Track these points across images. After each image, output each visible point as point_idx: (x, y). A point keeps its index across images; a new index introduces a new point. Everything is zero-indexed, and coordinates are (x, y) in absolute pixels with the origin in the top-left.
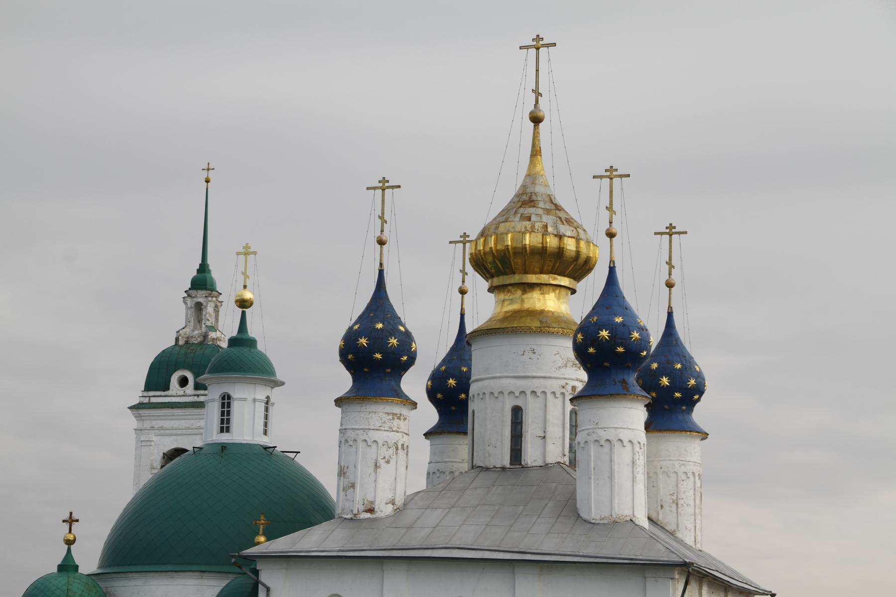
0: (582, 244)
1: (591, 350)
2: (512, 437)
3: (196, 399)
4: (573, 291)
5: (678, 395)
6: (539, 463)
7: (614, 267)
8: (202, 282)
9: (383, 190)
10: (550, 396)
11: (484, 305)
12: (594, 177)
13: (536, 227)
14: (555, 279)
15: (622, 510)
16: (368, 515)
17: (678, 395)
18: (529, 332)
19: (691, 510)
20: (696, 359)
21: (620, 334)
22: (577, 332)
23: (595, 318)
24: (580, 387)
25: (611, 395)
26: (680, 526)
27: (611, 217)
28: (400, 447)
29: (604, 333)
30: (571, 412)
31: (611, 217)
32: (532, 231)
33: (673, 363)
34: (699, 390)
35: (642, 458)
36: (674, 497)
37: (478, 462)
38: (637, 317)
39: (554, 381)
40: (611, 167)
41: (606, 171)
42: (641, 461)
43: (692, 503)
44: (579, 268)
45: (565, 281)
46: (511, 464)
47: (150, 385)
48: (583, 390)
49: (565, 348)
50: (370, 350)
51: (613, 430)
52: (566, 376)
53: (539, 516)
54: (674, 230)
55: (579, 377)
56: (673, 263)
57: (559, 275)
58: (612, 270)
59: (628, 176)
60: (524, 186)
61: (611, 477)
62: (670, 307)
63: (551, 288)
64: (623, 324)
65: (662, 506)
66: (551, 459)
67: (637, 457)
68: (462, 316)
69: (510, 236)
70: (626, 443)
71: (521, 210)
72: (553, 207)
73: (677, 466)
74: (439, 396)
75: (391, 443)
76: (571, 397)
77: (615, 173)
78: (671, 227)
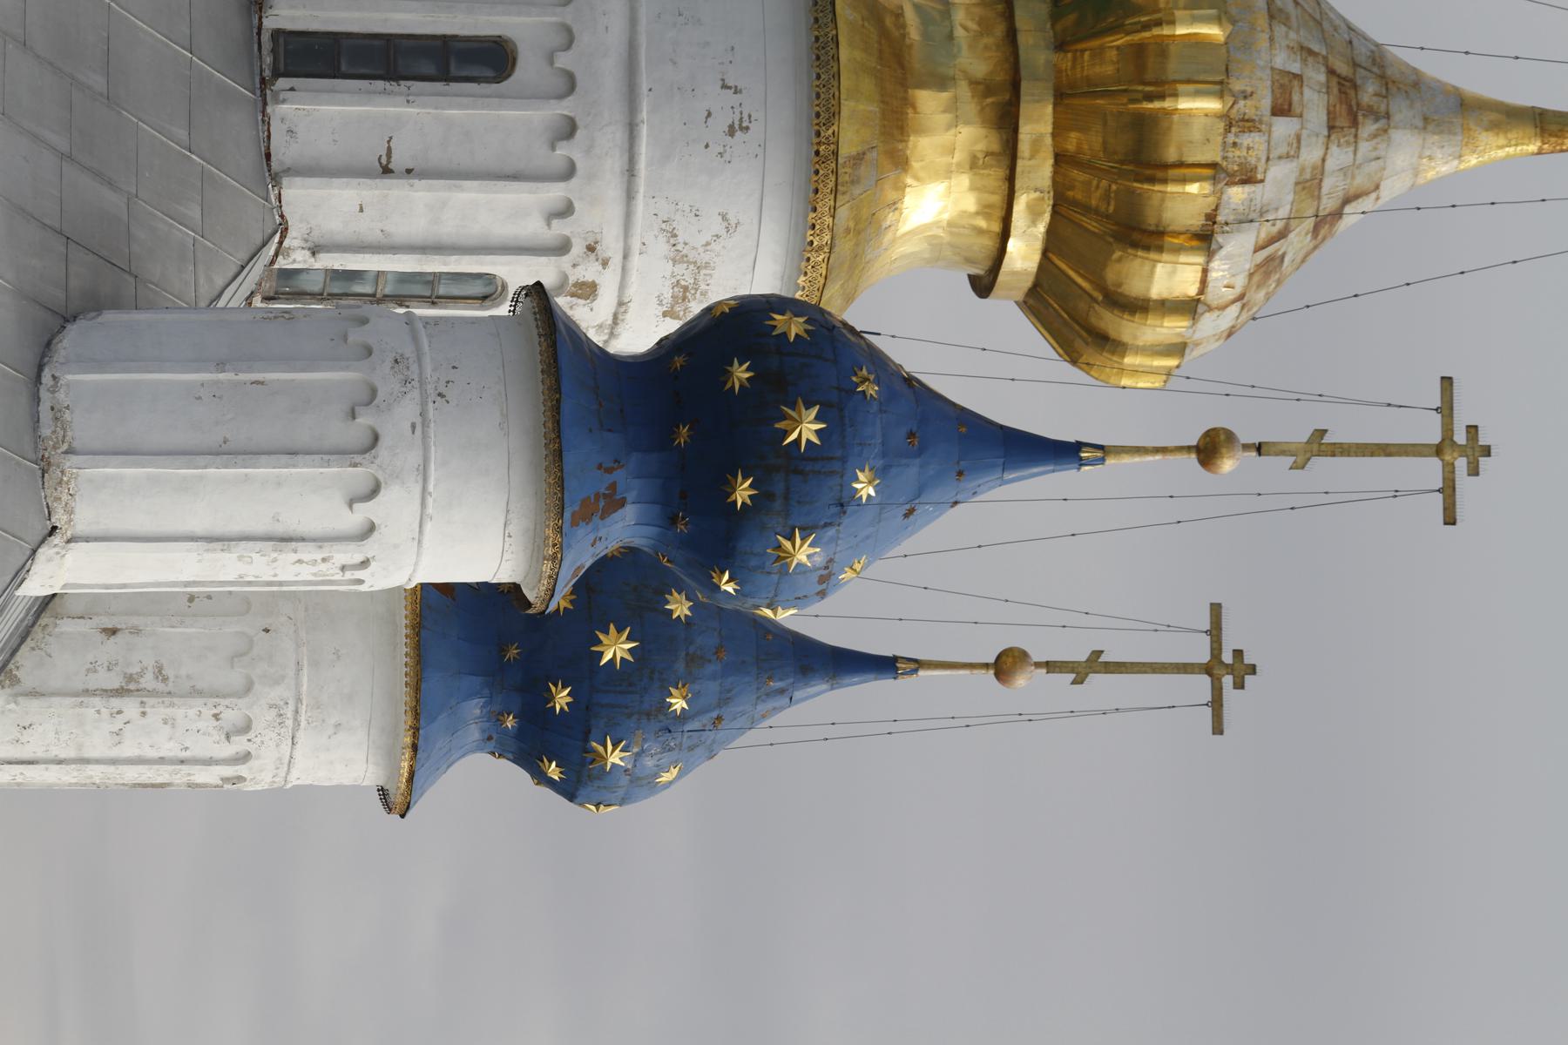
0: (1171, 328)
1: (741, 373)
2: (388, 39)
4: (983, 285)
5: (562, 698)
6: (283, 151)
7: (1082, 463)
9: (1207, 669)
10: (554, 193)
12: (1447, 382)
13: (1247, 140)
14: (1034, 215)
15: (98, 494)
17: (562, 698)
18: (822, 111)
19: (98, 745)
20: (705, 770)
21: (803, 490)
22: (816, 315)
23: (872, 390)
24: (590, 319)
25: (558, 456)
26: (35, 704)
29: (808, 429)
30: (489, 279)
32: (1233, 123)
33: (686, 680)
34: (580, 782)
35: (306, 573)
36: (148, 681)
38: (875, 555)
39: (615, 211)
40: (1487, 451)
41: (1472, 430)
42: (291, 569)
43: (128, 750)
44: (1077, 309)
45: (1023, 253)
46: (277, 34)
48: (576, 337)
49: (749, 263)
51: (414, 458)
52: (636, 260)
53: (67, 157)
54: (1228, 680)
55: (632, 319)
56: (1095, 680)
57: (1051, 232)
58: (1066, 453)
59: (1450, 520)
60: (1415, 85)
61: (226, 453)
62: (918, 664)
63: (997, 199)
64: (845, 502)
65: (113, 632)
66: (298, 196)
67: (309, 553)
69: (1214, 32)
70: (364, 511)
71: (1317, 76)
72: (1328, 204)
73: (276, 694)
76: (548, 282)
77: (1461, 464)
78: (1242, 670)
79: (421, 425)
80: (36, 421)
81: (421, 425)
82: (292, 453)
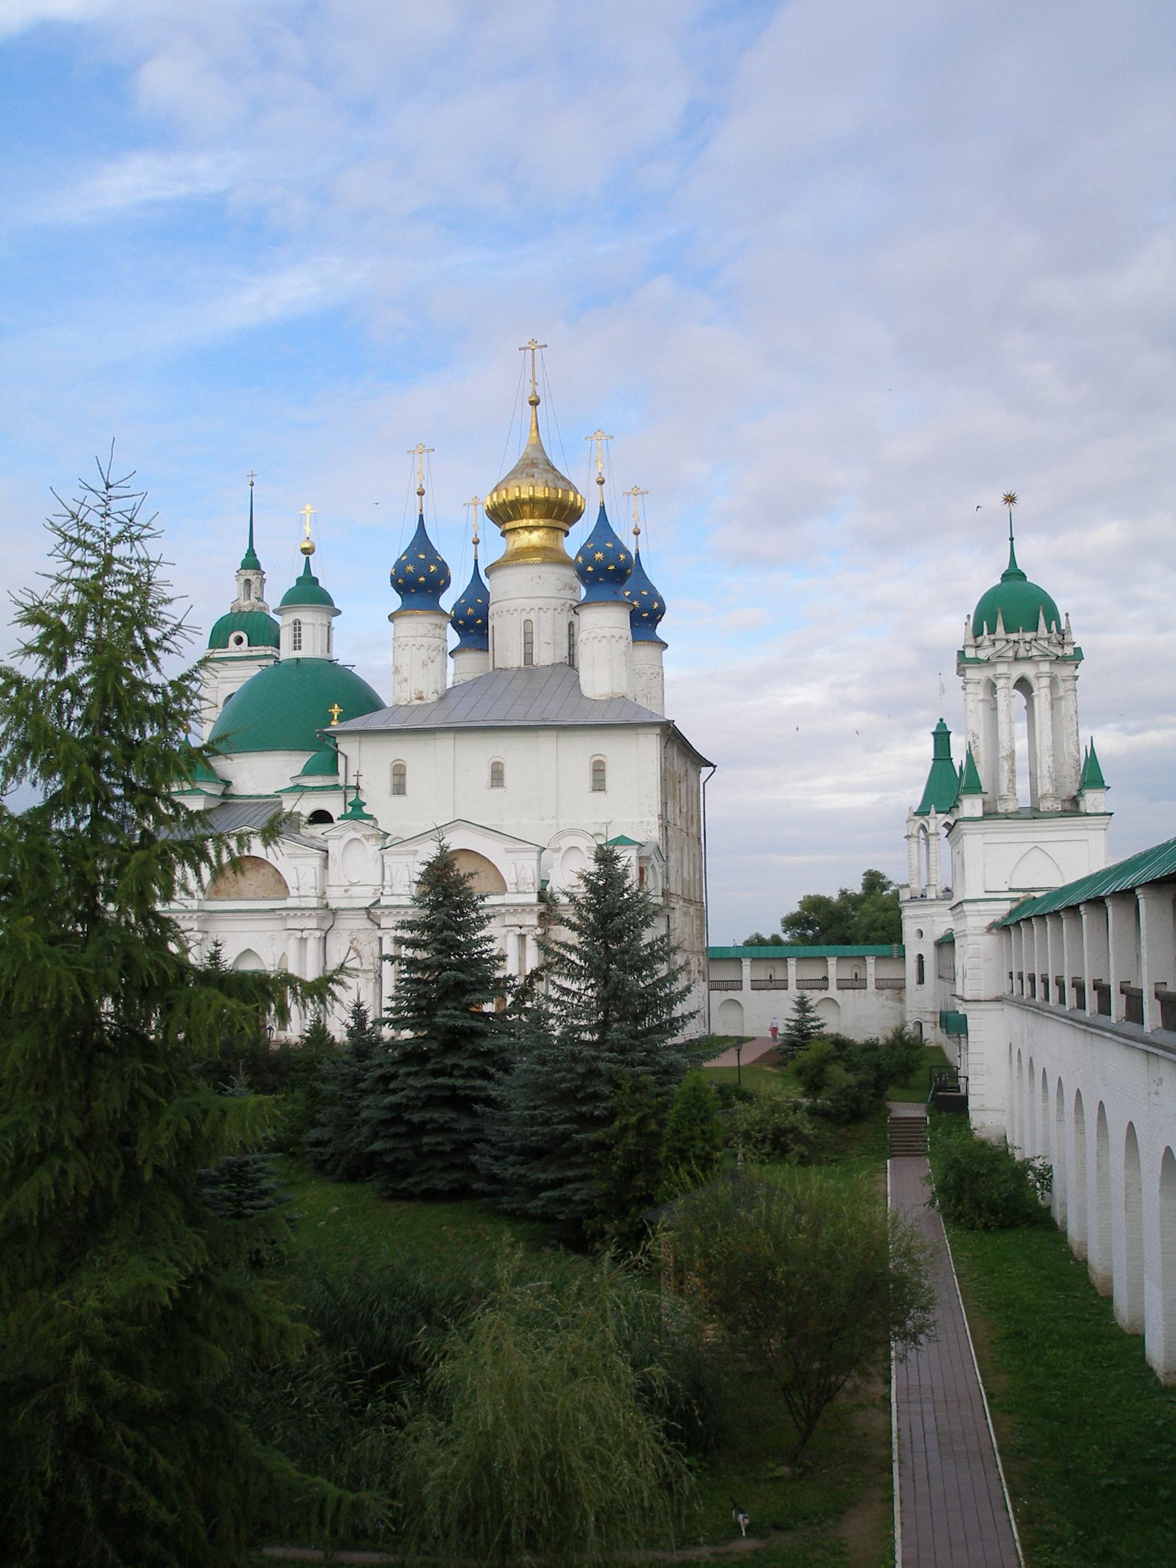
1: (590, 569)
3: (250, 654)
8: (251, 562)
11: (495, 546)
16: (419, 702)
34: (661, 611)
47: (212, 645)
68: (476, 561)
74: (461, 622)
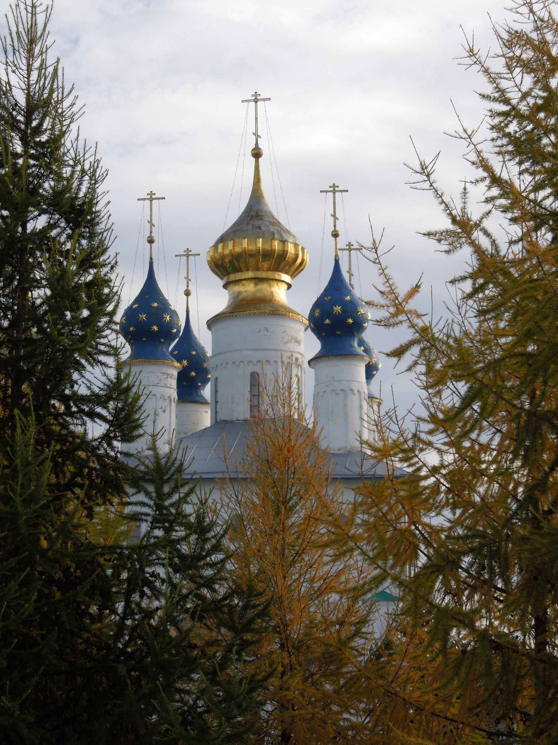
1: (327, 321)
12: (321, 191)
27: (188, 283)
28: (172, 399)
31: (188, 283)
37: (223, 416)
41: (330, 187)
50: (149, 324)
70: (356, 392)
75: (166, 397)
79: (339, 381)
80: (341, 454)
81: (339, 381)
82: (345, 405)
